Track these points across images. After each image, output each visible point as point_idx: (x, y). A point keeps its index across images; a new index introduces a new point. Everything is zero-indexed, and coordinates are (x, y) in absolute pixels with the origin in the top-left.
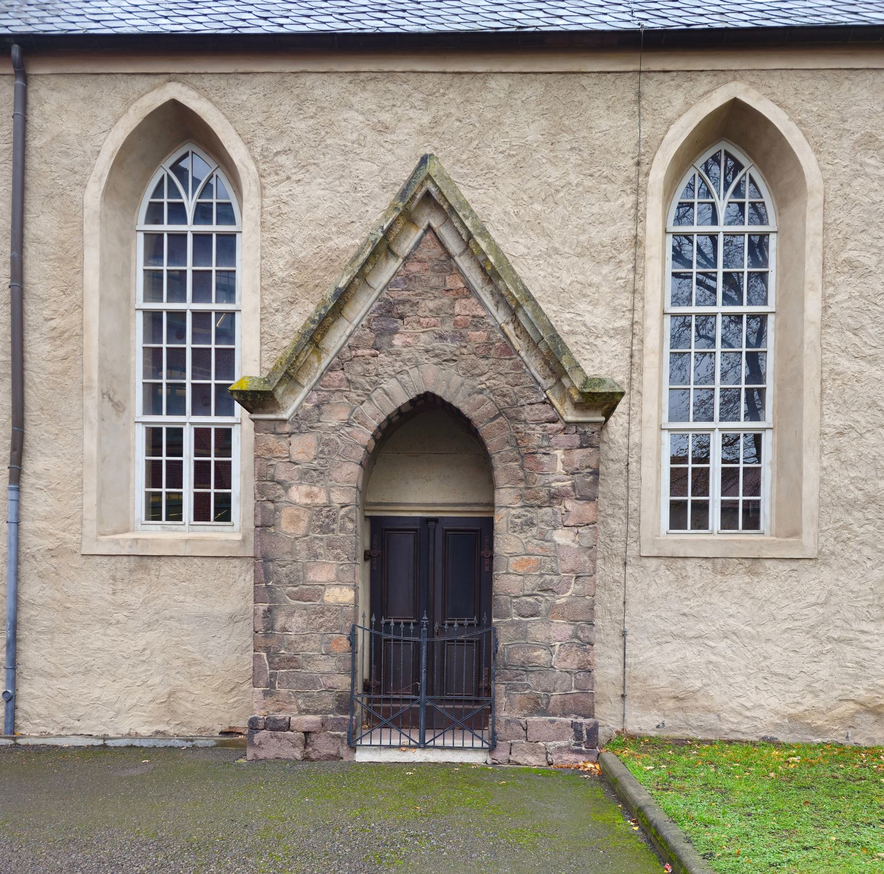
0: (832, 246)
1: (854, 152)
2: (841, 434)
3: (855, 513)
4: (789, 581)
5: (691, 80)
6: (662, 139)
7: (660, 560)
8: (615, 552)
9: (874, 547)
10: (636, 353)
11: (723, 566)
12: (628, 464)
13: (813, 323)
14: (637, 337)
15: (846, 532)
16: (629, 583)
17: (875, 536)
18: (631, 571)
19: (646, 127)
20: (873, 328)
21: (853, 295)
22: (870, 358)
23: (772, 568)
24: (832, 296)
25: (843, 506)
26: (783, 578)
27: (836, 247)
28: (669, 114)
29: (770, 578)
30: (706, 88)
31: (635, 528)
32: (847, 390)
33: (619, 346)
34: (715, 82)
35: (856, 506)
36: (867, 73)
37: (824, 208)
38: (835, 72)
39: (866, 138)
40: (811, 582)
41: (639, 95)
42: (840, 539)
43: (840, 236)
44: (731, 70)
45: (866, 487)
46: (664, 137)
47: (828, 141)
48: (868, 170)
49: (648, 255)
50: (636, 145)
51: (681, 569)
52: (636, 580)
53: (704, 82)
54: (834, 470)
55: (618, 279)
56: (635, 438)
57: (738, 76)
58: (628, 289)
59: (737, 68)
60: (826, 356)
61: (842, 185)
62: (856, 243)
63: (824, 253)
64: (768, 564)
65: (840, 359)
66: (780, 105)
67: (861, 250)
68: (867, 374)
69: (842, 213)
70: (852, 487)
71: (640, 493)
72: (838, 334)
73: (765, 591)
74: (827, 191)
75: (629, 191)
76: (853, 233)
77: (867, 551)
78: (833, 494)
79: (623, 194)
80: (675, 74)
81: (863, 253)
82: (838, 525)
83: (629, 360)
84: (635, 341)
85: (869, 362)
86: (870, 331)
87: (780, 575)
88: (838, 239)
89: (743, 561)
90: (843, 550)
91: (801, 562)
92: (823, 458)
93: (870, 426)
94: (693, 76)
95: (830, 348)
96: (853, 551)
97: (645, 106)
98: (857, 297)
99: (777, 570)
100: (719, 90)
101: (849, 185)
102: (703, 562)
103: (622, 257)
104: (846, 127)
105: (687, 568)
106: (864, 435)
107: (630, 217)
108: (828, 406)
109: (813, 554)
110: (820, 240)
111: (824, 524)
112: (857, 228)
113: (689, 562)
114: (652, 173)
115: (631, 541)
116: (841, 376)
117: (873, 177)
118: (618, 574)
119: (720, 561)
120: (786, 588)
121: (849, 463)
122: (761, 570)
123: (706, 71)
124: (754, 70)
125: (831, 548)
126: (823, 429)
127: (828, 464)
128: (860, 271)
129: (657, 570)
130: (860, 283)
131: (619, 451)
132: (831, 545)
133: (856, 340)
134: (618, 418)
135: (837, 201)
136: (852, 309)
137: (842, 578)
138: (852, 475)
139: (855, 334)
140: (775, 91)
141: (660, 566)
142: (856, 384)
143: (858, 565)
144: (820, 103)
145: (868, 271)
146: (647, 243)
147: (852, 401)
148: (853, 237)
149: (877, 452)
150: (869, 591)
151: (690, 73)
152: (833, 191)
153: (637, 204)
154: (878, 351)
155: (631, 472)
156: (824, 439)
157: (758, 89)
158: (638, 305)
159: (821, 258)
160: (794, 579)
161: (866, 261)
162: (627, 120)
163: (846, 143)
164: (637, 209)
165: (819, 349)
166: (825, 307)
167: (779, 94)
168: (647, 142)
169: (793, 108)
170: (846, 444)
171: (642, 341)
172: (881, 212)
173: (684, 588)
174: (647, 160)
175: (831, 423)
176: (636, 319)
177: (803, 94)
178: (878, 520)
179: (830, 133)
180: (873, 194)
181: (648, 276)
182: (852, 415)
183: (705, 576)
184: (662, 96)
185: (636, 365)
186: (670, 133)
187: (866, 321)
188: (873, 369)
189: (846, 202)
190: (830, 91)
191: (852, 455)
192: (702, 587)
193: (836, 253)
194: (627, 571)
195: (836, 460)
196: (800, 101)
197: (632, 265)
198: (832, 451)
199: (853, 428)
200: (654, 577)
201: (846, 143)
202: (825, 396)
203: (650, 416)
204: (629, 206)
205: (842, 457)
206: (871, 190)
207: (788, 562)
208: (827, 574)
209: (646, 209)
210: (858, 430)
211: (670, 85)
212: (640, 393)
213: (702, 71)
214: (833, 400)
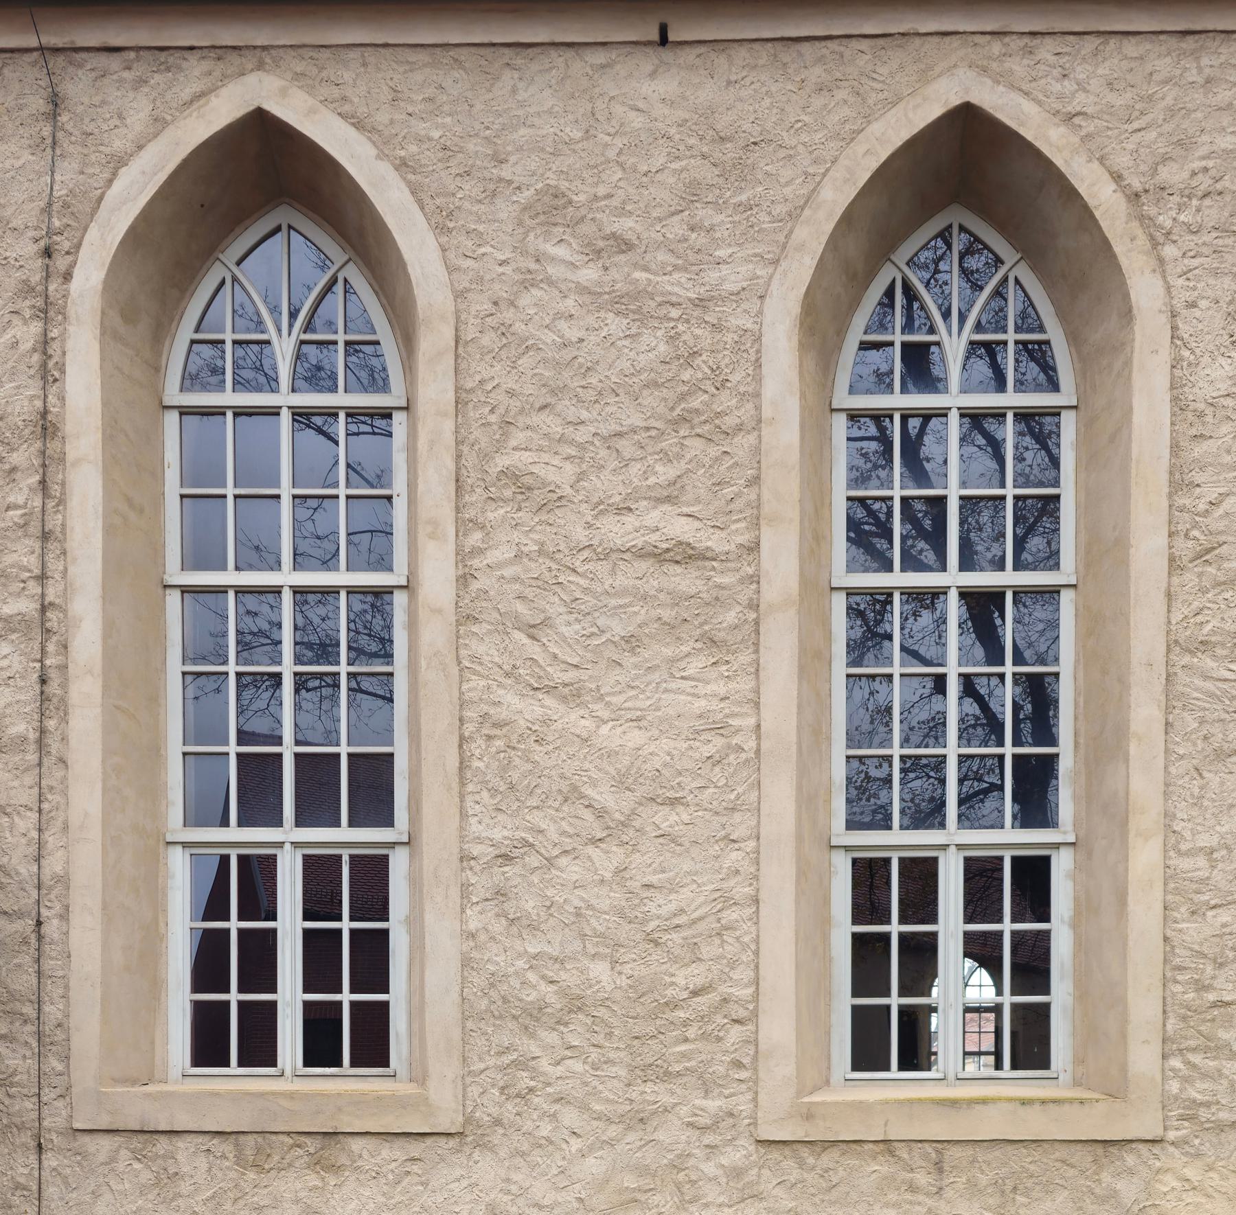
0: (476, 441)
1: (521, 230)
2: (506, 858)
3: (543, 1034)
4: (404, 1184)
5: (168, 69)
6: (100, 199)
7: (118, 1139)
8: (17, 1120)
9: (584, 1107)
10: (53, 674)
11: (259, 1150)
12: (39, 923)
13: (439, 611)
14: (54, 639)
15: (525, 1074)
16: (51, 1191)
17: (586, 1084)
18: (54, 1164)
19: (67, 174)
20: (569, 624)
21: (525, 549)
22: (566, 690)
23: (365, 1154)
24: (477, 552)
25: (514, 1017)
26: (391, 1177)
27: (484, 443)
28: (118, 145)
29: (362, 1177)
30: (195, 87)
31: (60, 1067)
32: (517, 761)
33: (16, 658)
34: (217, 73)
35: (544, 1019)
36: (553, 53)
37: (457, 356)
38: (482, 51)
39: (546, 199)
40: (452, 1186)
41: (55, 102)
42: (512, 1091)
43: (493, 418)
44: (255, 47)
45: (563, 975)
46: (103, 194)
47: (467, 205)
48: (553, 270)
49: (71, 456)
50: (43, 210)
51: (164, 1157)
52: (67, 1184)
53: (195, 72)
54: (493, 938)
55: (8, 508)
56: (54, 864)
57: (268, 60)
58: (31, 530)
59: (266, 43)
60: (471, 684)
61: (496, 303)
62: (529, 433)
63: (459, 457)
64: (357, 1145)
65: (501, 692)
66: (359, 125)
67: (540, 449)
68: (559, 725)
69: (498, 368)
70: (532, 977)
71: (67, 987)
72: (497, 638)
73: (353, 1206)
74: (463, 317)
75: (27, 313)
76: (522, 411)
77: (570, 1117)
78: (492, 993)
79: (16, 320)
80: (132, 55)
81: (546, 457)
82: (506, 1059)
83: (37, 688)
84: (51, 647)
85: (564, 699)
86: (563, 629)
87: (384, 1170)
88: (489, 424)
89: (303, 1139)
90: (518, 1114)
91: (429, 1141)
92: (469, 912)
93: (567, 840)
94: (172, 59)
95: (478, 668)
96: (540, 1118)
97: (68, 127)
98: (534, 555)
99: (378, 1160)
100: (224, 92)
101: (512, 304)
102: (215, 1141)
103: (17, 458)
104: (503, 174)
105: (179, 1157)
106: (555, 862)
107: (32, 372)
108: (477, 797)
109: (453, 1123)
110: (449, 425)
111: (475, 1058)
112: (531, 399)
113: (181, 1143)
114: (77, 273)
115: (53, 1096)
116: (505, 730)
117: (563, 287)
118: (26, 1171)
119: (250, 1139)
120: (398, 1198)
121: (525, 922)
122: (343, 1160)
123: (201, 48)
124: (304, 46)
125: (495, 1111)
126: (466, 846)
127: (480, 926)
128: (538, 496)
129: (112, 1160)
130: (540, 523)
131: (22, 894)
132: (491, 1105)
133: (534, 650)
134: (16, 819)
135: (486, 340)
136: (522, 583)
137: (516, 1177)
138: (531, 950)
139: (533, 638)
140: (349, 92)
141: (117, 1151)
142: (537, 747)
143: (550, 1148)
144: (448, 120)
145: (555, 496)
146: (69, 428)
147: (528, 786)
148: (522, 421)
149: (582, 899)
150: (576, 1205)
151: (165, 54)
152: (476, 317)
153: (46, 343)
154: (584, 675)
155: (48, 940)
156: (471, 869)
157: (310, 90)
158: (55, 566)
159: (451, 465)
160: (417, 1179)
161: (551, 475)
162: (26, 156)
163: (505, 210)
164: (45, 353)
165: (455, 670)
166: (464, 576)
167: (356, 100)
168: (66, 205)
169: (386, 133)
170: (519, 880)
171: (66, 647)
172: (581, 366)
173: (172, 1200)
174: (66, 245)
175: (484, 835)
176: (49, 599)
177: (410, 101)
178: (592, 1049)
179: (470, 188)
180: (562, 325)
181: (74, 503)
182: (528, 818)
183: (220, 1175)
184: (104, 102)
185: (55, 700)
186: (117, 186)
187: (554, 607)
188: (573, 716)
189: (504, 341)
190: (469, 94)
191: (530, 905)
192: (213, 1197)
193: (486, 457)
194: (45, 1163)
195: (498, 915)
196: (404, 116)
197: (38, 478)
198: (488, 896)
199: (531, 845)
200: (105, 1176)
201: (505, 210)
202: (469, 775)
203: (86, 815)
204: (29, 345)
205: (511, 908)
206: (558, 316)
207: (401, 1142)
208: (486, 1168)
209: (64, 353)
210: (543, 851)
211: (121, 81)
212: (62, 761)
213: (192, 48)
214: (487, 782)
